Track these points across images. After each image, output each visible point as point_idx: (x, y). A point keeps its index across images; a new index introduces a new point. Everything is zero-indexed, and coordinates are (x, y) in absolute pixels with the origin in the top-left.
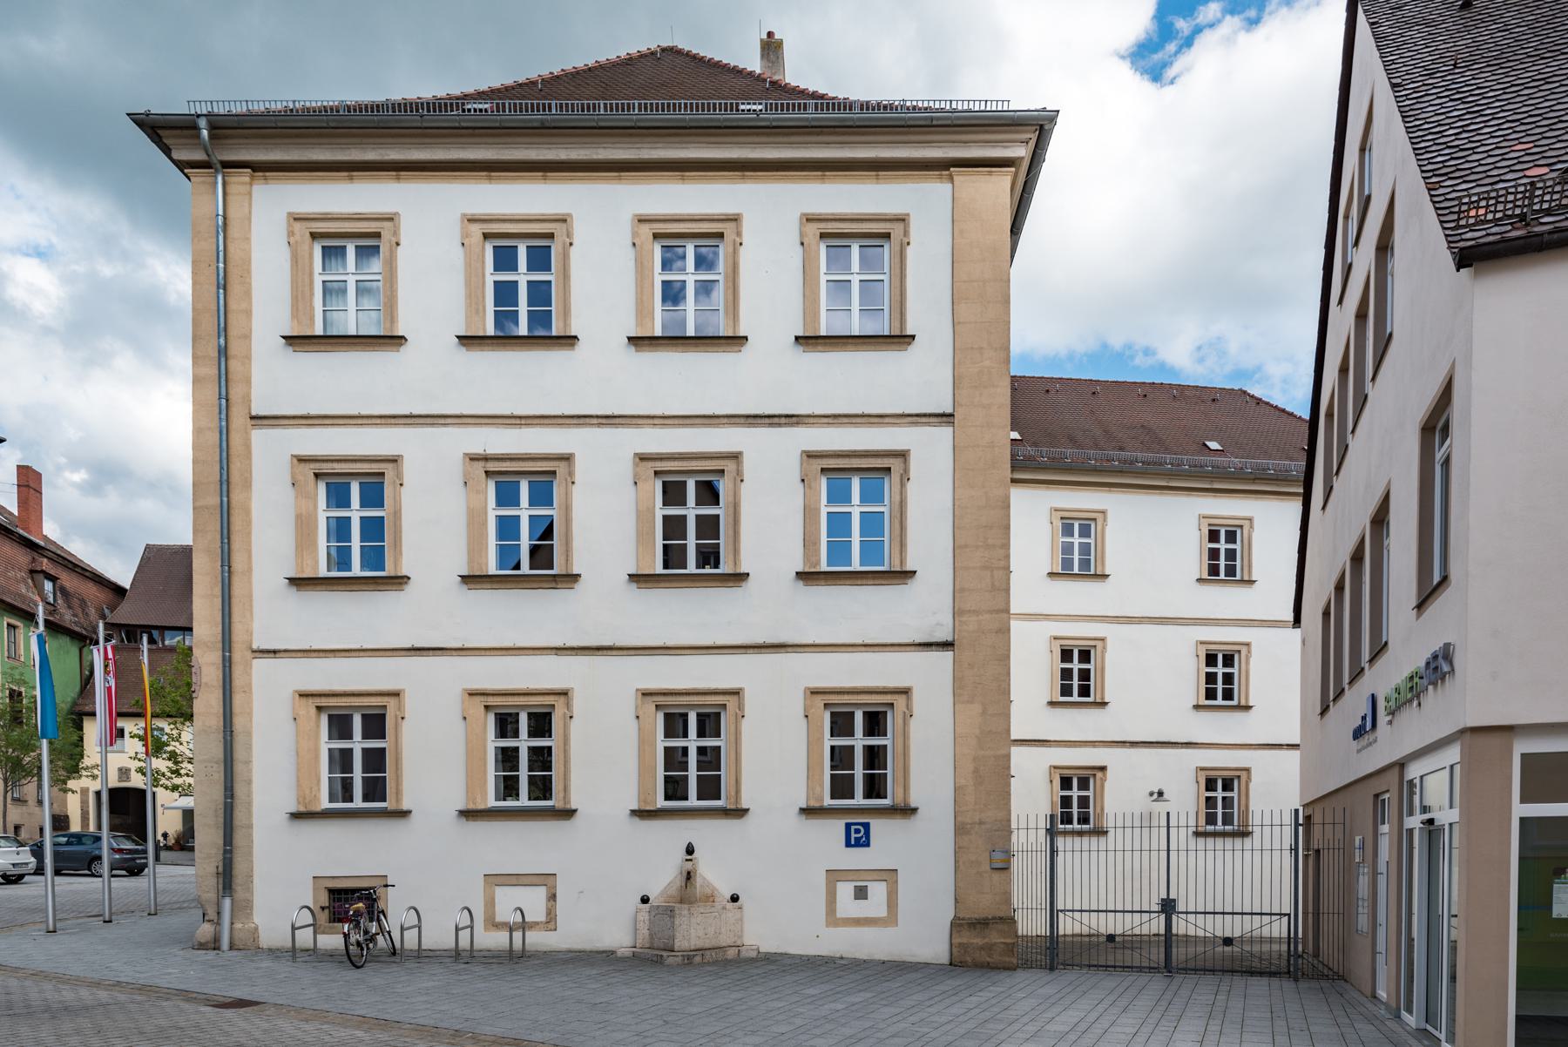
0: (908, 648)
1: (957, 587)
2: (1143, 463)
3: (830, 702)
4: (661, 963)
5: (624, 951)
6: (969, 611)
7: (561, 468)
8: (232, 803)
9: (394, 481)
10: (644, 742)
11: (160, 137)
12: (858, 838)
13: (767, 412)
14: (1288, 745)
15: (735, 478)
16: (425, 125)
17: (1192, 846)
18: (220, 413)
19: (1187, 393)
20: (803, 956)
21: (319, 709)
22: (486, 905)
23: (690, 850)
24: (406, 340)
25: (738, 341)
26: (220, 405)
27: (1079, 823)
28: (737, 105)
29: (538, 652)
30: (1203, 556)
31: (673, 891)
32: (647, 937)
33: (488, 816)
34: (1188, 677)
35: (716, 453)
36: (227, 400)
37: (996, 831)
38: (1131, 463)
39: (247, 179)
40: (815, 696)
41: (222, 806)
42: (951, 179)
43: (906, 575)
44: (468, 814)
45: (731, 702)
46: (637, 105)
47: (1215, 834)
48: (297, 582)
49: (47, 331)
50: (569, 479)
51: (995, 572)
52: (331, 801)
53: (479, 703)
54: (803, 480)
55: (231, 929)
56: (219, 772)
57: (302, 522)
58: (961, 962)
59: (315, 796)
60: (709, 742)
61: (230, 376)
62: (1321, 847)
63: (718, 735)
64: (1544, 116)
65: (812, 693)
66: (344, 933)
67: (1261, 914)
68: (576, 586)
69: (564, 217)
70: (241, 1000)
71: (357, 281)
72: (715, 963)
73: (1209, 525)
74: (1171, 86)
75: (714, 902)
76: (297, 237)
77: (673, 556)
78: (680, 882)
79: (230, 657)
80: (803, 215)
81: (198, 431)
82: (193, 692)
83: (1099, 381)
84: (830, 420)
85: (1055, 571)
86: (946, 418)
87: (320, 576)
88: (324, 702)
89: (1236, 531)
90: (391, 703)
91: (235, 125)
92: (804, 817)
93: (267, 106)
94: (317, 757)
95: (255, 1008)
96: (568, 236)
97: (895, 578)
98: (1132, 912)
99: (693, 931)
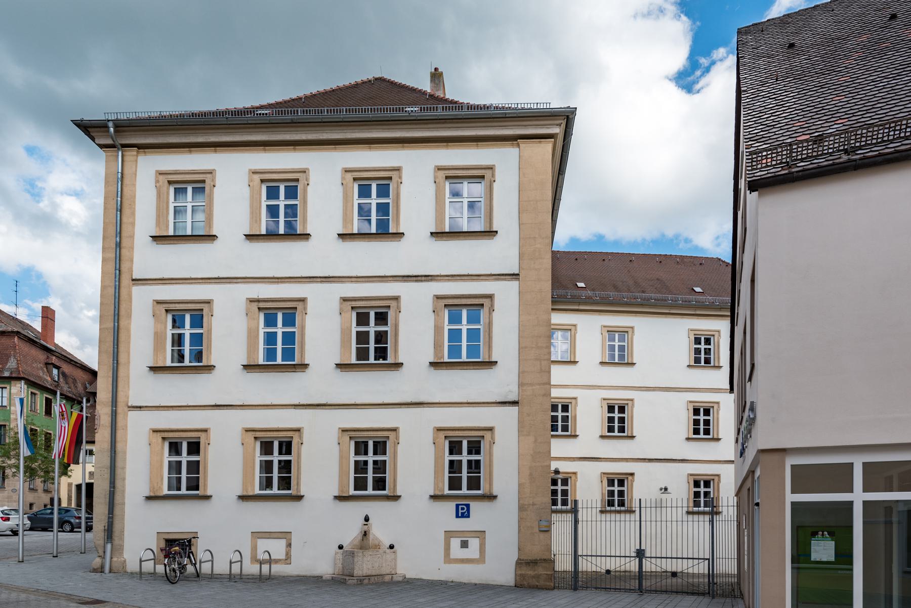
0: (493, 405)
1: (520, 370)
2: (655, 300)
4: (345, 583)
5: (328, 577)
6: (528, 383)
7: (300, 306)
8: (114, 491)
9: (208, 314)
10: (343, 458)
12: (463, 513)
13: (415, 274)
15: (396, 311)
16: (229, 123)
17: (599, 519)
18: (115, 278)
19: (685, 260)
20: (429, 580)
21: (164, 439)
22: (252, 549)
23: (367, 519)
24: (217, 237)
25: (718, 439)
26: (116, 273)
27: (619, 506)
28: (403, 108)
29: (285, 407)
30: (691, 353)
31: (357, 542)
32: (341, 568)
33: (254, 499)
34: (683, 422)
35: (385, 297)
36: (120, 271)
37: (542, 509)
38: (648, 300)
39: (135, 153)
40: (439, 432)
41: (108, 493)
42: (518, 146)
43: (492, 364)
44: (243, 498)
45: (392, 435)
46: (344, 110)
47: (699, 513)
48: (154, 369)
49: (78, 234)
50: (304, 311)
51: (543, 362)
52: (169, 490)
53: (251, 435)
54: (434, 311)
55: (111, 562)
56: (107, 474)
57: (157, 335)
58: (521, 585)
59: (160, 487)
60: (379, 458)
61: (122, 258)
63: (385, 453)
64: (815, 107)
65: (438, 430)
66: (165, 564)
67: (693, 559)
68: (306, 370)
69: (305, 170)
70: (97, 600)
71: (192, 206)
72: (376, 584)
73: (695, 335)
74: (698, 94)
75: (379, 548)
76: (161, 183)
77: (362, 354)
78: (360, 537)
79: (116, 410)
80: (436, 166)
81: (103, 288)
82: (96, 429)
83: (634, 254)
84: (450, 278)
85: (604, 361)
86: (515, 276)
87: (167, 365)
88: (166, 435)
89: (710, 338)
90: (202, 436)
91: (128, 125)
92: (432, 500)
93: (149, 114)
95: (102, 605)
96: (307, 180)
97: (485, 365)
98: (610, 556)
99: (365, 565)
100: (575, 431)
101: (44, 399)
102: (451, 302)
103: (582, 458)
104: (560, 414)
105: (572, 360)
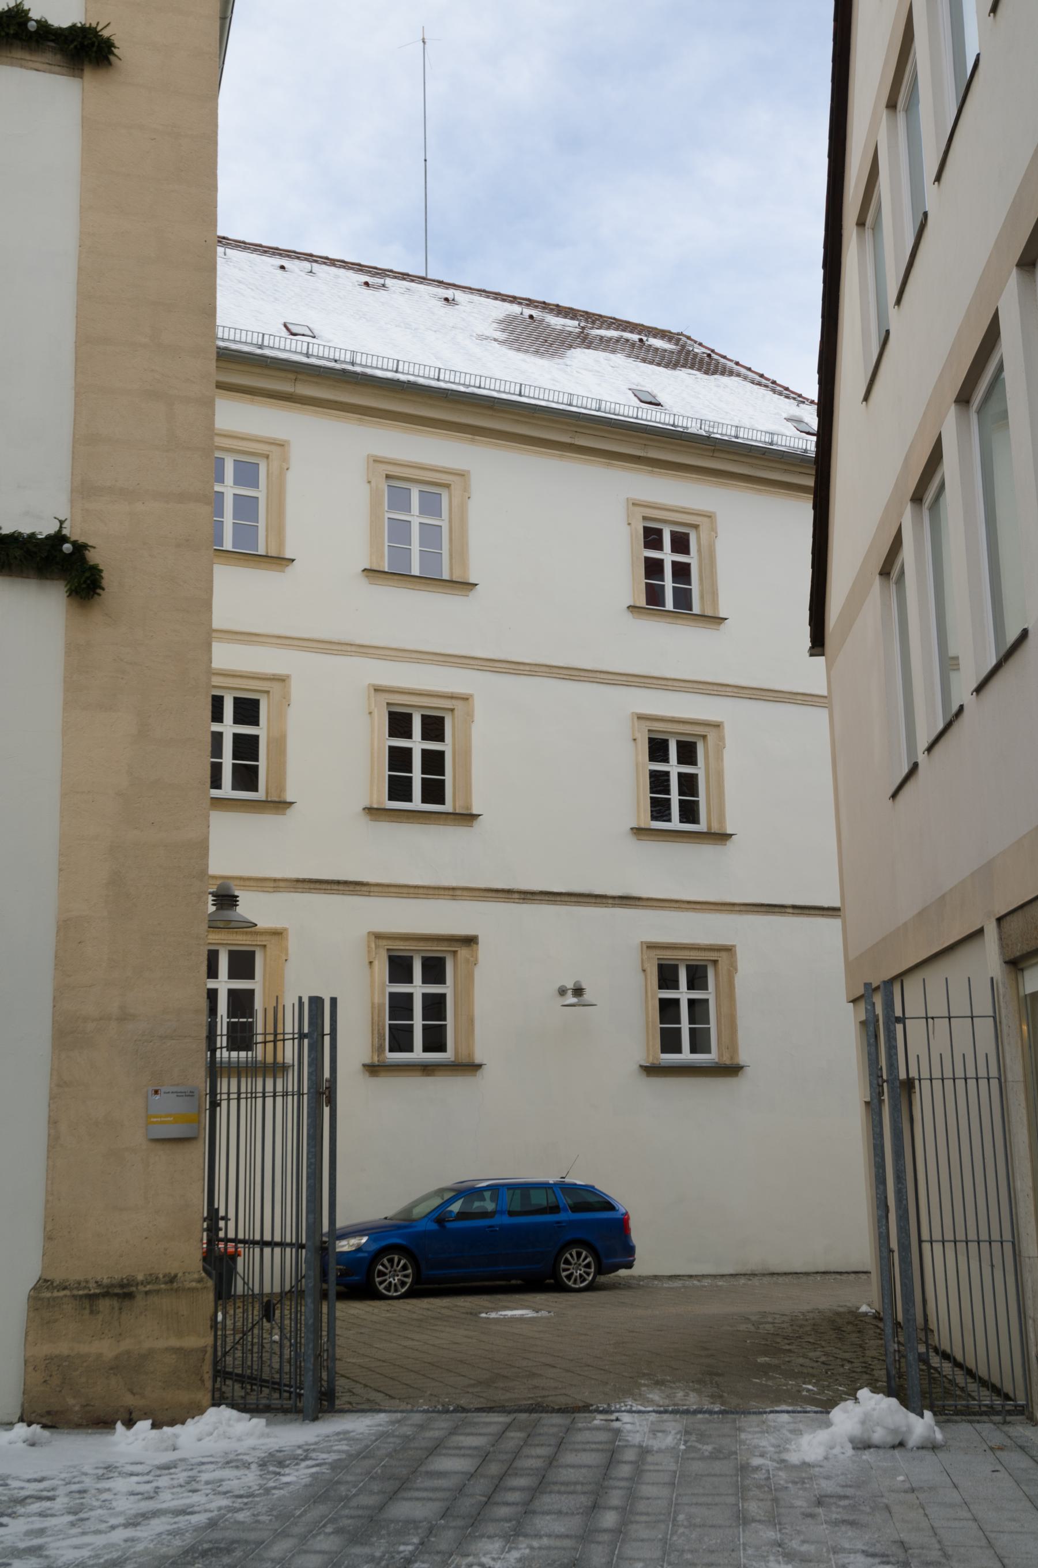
14: (794, 907)
62: (913, 1073)
73: (645, 518)
103: (304, 881)
105: (273, 553)
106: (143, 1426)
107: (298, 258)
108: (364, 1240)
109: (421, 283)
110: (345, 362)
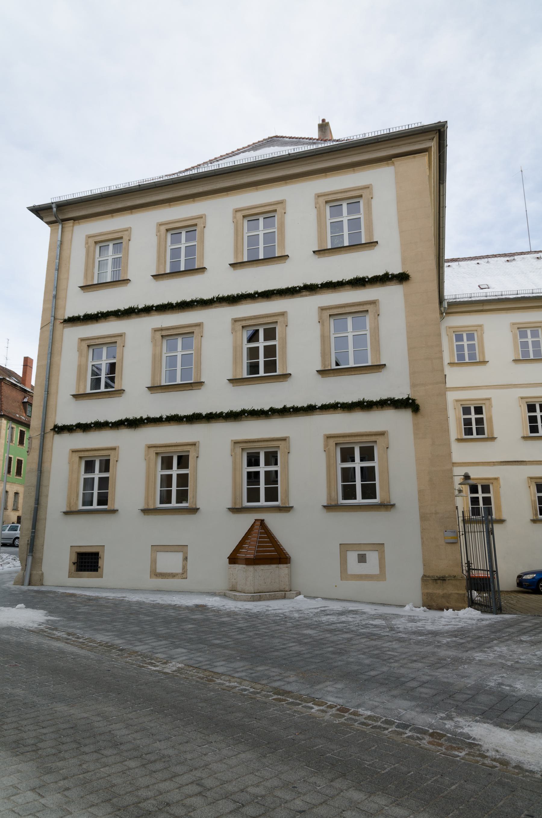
3: (339, 442)
11: (39, 213)
22: (151, 563)
25: (127, 281)
35: (273, 313)
48: (76, 396)
53: (153, 451)
63: (276, 464)
94: (78, 483)
100: (484, 357)
101: (19, 431)
102: (165, 333)
103: (503, 462)
104: (473, 416)
106: (450, 610)
107: (483, 258)
108: (535, 575)
109: (528, 254)
110: (499, 295)
